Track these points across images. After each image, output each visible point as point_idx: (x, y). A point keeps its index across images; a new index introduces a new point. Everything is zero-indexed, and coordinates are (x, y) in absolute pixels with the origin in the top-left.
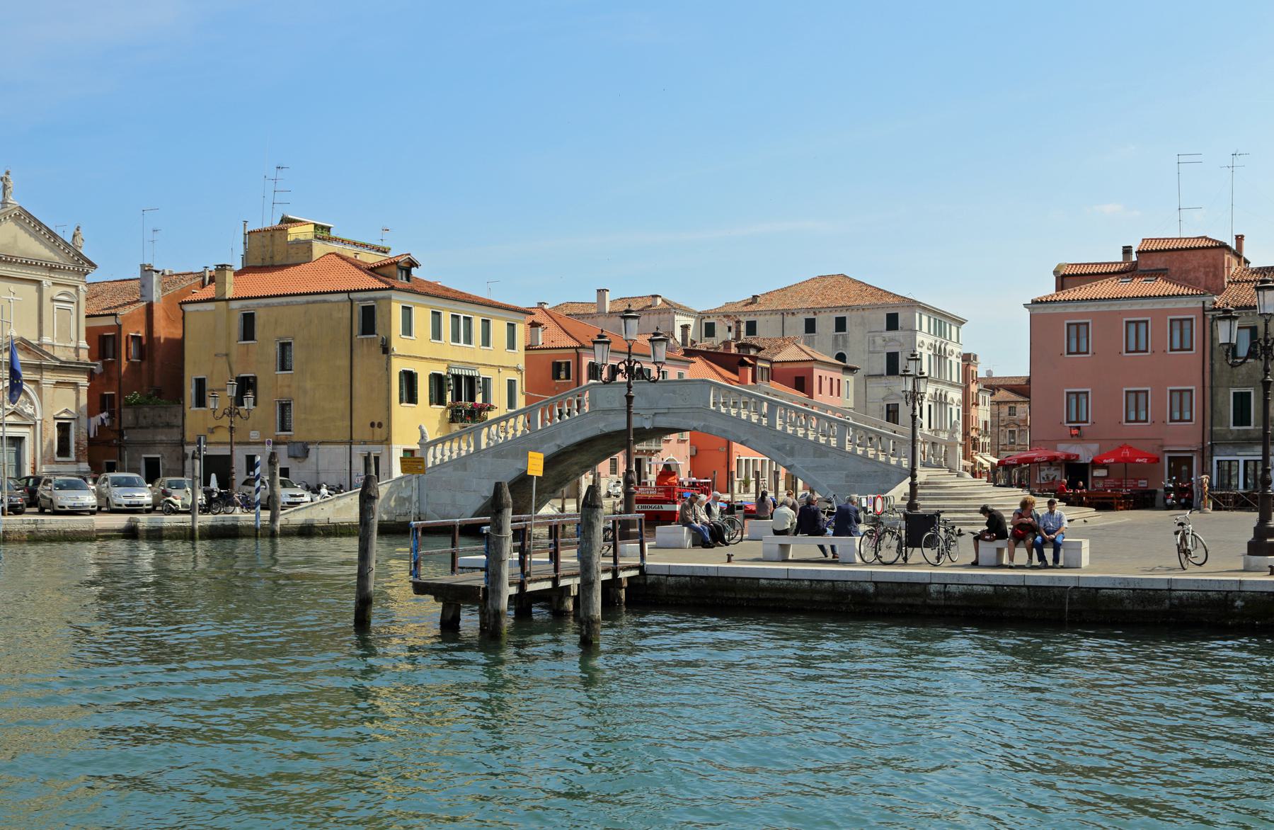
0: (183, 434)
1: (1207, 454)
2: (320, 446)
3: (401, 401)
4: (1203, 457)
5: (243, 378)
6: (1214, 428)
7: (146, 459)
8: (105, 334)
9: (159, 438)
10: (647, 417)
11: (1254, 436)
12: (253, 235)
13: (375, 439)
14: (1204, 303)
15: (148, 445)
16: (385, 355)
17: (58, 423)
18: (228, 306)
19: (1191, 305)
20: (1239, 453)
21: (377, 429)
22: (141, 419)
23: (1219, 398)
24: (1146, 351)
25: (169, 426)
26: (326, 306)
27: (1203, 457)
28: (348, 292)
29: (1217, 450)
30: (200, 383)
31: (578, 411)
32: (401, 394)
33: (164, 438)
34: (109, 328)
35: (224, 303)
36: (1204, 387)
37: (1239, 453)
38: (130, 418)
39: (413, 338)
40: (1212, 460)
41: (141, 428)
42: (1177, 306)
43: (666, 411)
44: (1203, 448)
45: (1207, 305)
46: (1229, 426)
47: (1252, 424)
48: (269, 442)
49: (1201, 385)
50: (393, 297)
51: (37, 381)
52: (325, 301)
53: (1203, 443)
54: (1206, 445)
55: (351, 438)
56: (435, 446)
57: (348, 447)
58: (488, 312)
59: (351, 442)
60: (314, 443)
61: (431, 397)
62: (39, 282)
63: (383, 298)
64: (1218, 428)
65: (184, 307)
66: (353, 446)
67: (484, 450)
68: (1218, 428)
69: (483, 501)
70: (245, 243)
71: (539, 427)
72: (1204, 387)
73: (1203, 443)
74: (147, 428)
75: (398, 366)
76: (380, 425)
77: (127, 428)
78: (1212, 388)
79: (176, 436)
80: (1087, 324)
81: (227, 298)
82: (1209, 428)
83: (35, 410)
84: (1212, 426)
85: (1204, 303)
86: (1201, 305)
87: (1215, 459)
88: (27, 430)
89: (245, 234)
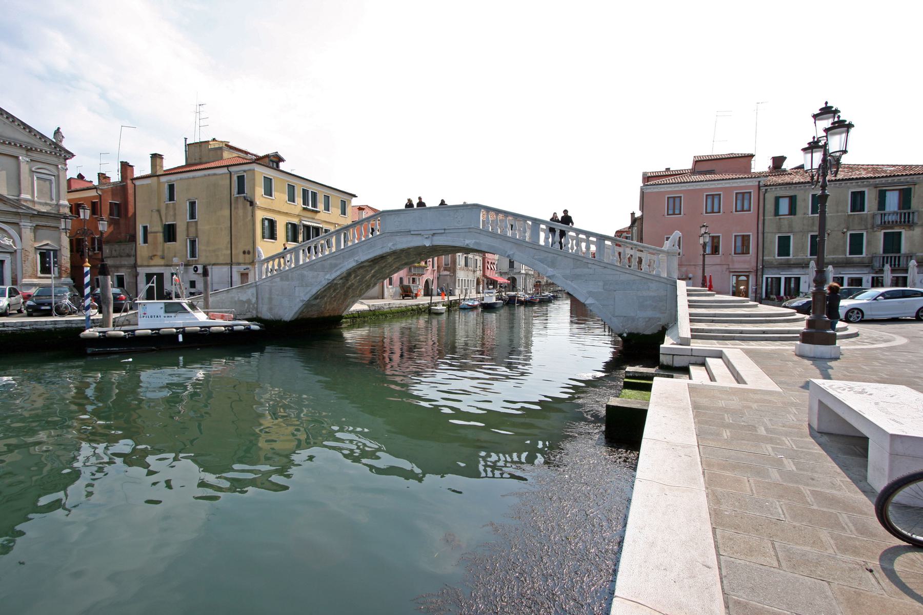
0: (136, 261)
1: (759, 273)
2: (213, 267)
3: (263, 237)
4: (757, 275)
5: (169, 225)
6: (765, 258)
7: (117, 276)
8: (93, 201)
9: (123, 263)
10: (427, 236)
11: (792, 262)
12: (189, 146)
13: (246, 262)
14: (759, 182)
15: (117, 267)
16: (251, 207)
17: (40, 252)
18: (159, 180)
19: (750, 184)
20: (781, 273)
21: (247, 255)
22: (113, 252)
23: (767, 240)
24: (719, 212)
25: (129, 256)
26: (215, 177)
27: (757, 275)
28: (227, 166)
29: (766, 270)
30: (145, 228)
31: (372, 234)
32: (263, 233)
33: (126, 263)
34: (94, 197)
35: (156, 178)
36: (758, 233)
37: (781, 273)
38: (107, 251)
39: (273, 198)
40: (762, 277)
41: (114, 257)
42: (749, 184)
43: (443, 231)
44: (757, 270)
45: (761, 184)
46: (774, 257)
47: (791, 255)
48: (182, 264)
49: (756, 231)
50: (256, 169)
51: (18, 224)
52: (215, 174)
53: (757, 266)
54: (759, 268)
55: (232, 261)
56: (274, 260)
57: (229, 267)
58: (328, 192)
59: (231, 264)
60: (209, 265)
61: (287, 236)
62: (17, 158)
63: (250, 170)
64: (768, 258)
65: (134, 181)
66: (233, 266)
67: (302, 265)
68: (768, 258)
69: (301, 304)
70: (186, 151)
71: (342, 247)
72: (758, 233)
73: (757, 266)
74: (117, 257)
75: (260, 215)
76: (249, 253)
77: (106, 257)
78: (763, 233)
79: (131, 261)
80: (680, 197)
81: (158, 174)
82: (761, 258)
83: (14, 242)
84: (763, 257)
85: (759, 182)
86: (757, 183)
87: (765, 276)
88: (8, 256)
89: (186, 146)
